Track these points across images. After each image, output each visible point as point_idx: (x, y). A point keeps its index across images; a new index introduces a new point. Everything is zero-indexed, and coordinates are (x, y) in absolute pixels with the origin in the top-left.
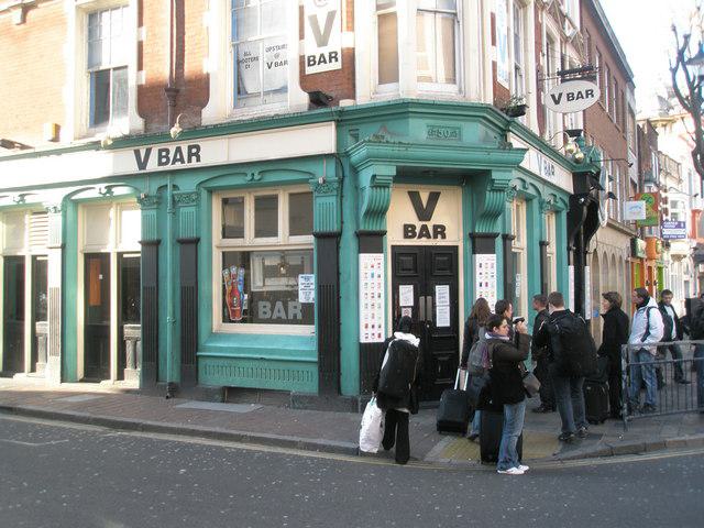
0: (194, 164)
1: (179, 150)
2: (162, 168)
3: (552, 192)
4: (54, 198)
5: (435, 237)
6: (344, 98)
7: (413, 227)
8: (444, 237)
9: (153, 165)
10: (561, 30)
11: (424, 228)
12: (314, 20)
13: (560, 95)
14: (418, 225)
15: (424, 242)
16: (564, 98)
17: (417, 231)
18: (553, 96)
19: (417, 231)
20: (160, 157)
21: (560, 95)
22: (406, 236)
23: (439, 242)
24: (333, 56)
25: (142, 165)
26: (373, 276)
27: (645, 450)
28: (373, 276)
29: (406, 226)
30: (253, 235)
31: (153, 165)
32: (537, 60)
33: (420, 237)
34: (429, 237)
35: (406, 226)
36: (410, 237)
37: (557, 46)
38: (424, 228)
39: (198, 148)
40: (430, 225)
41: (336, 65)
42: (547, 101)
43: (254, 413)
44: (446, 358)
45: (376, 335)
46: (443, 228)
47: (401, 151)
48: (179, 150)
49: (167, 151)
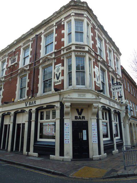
0: (35, 105)
1: (32, 102)
2: (29, 106)
3: (114, 109)
4: (13, 112)
5: (82, 119)
6: (62, 89)
7: (77, 117)
8: (84, 119)
9: (28, 105)
10: (116, 77)
11: (80, 117)
12: (57, 74)
13: (114, 89)
14: (78, 116)
15: (80, 120)
16: (115, 89)
17: (78, 117)
18: (113, 89)
19: (78, 117)
20: (29, 104)
21: (114, 89)
22: (75, 119)
23: (83, 120)
24: (60, 81)
25: (26, 105)
26: (67, 128)
27: (129, 176)
28: (67, 128)
29: (75, 117)
30: (51, 118)
31: (28, 105)
32: (109, 81)
33: (79, 119)
34: (81, 119)
35: (75, 117)
36: (77, 119)
37: (115, 80)
38: (80, 117)
39: (35, 101)
40: (81, 116)
41: (60, 83)
42: (111, 90)
43: (41, 161)
44: (86, 148)
45: (68, 142)
46: (84, 117)
47: (72, 100)
48: (32, 102)
49: (30, 102)
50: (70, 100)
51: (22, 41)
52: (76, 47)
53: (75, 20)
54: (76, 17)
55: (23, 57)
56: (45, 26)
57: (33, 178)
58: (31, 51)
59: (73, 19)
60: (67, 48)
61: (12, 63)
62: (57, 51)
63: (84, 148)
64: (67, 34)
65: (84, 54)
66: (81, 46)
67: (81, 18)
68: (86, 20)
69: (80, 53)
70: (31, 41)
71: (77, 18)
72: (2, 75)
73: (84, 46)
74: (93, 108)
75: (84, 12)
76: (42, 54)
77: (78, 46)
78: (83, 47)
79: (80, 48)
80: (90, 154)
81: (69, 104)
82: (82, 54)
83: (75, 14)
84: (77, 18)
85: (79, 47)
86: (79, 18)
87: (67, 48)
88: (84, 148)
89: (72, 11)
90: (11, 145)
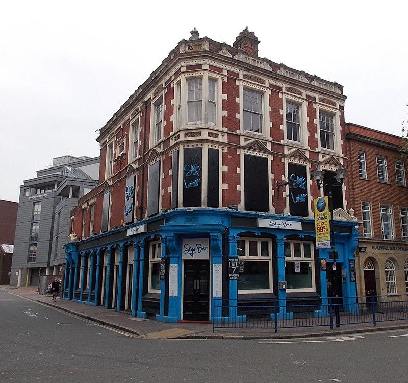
50: (174, 228)
51: (130, 110)
52: (187, 135)
53: (187, 79)
54: (188, 74)
55: (155, 123)
56: (153, 86)
57: (194, 344)
58: (165, 112)
59: (182, 78)
60: (187, 132)
61: (120, 151)
63: (202, 304)
65: (199, 146)
67: (197, 75)
68: (206, 76)
69: (197, 145)
70: (165, 88)
71: (191, 75)
72: (136, 156)
73: (198, 131)
75: (202, 61)
76: (152, 143)
77: (190, 131)
79: (194, 134)
80: (322, 281)
81: (171, 235)
82: (195, 146)
83: (187, 67)
84: (191, 75)
86: (194, 74)
87: (187, 132)
88: (202, 304)
89: (182, 63)
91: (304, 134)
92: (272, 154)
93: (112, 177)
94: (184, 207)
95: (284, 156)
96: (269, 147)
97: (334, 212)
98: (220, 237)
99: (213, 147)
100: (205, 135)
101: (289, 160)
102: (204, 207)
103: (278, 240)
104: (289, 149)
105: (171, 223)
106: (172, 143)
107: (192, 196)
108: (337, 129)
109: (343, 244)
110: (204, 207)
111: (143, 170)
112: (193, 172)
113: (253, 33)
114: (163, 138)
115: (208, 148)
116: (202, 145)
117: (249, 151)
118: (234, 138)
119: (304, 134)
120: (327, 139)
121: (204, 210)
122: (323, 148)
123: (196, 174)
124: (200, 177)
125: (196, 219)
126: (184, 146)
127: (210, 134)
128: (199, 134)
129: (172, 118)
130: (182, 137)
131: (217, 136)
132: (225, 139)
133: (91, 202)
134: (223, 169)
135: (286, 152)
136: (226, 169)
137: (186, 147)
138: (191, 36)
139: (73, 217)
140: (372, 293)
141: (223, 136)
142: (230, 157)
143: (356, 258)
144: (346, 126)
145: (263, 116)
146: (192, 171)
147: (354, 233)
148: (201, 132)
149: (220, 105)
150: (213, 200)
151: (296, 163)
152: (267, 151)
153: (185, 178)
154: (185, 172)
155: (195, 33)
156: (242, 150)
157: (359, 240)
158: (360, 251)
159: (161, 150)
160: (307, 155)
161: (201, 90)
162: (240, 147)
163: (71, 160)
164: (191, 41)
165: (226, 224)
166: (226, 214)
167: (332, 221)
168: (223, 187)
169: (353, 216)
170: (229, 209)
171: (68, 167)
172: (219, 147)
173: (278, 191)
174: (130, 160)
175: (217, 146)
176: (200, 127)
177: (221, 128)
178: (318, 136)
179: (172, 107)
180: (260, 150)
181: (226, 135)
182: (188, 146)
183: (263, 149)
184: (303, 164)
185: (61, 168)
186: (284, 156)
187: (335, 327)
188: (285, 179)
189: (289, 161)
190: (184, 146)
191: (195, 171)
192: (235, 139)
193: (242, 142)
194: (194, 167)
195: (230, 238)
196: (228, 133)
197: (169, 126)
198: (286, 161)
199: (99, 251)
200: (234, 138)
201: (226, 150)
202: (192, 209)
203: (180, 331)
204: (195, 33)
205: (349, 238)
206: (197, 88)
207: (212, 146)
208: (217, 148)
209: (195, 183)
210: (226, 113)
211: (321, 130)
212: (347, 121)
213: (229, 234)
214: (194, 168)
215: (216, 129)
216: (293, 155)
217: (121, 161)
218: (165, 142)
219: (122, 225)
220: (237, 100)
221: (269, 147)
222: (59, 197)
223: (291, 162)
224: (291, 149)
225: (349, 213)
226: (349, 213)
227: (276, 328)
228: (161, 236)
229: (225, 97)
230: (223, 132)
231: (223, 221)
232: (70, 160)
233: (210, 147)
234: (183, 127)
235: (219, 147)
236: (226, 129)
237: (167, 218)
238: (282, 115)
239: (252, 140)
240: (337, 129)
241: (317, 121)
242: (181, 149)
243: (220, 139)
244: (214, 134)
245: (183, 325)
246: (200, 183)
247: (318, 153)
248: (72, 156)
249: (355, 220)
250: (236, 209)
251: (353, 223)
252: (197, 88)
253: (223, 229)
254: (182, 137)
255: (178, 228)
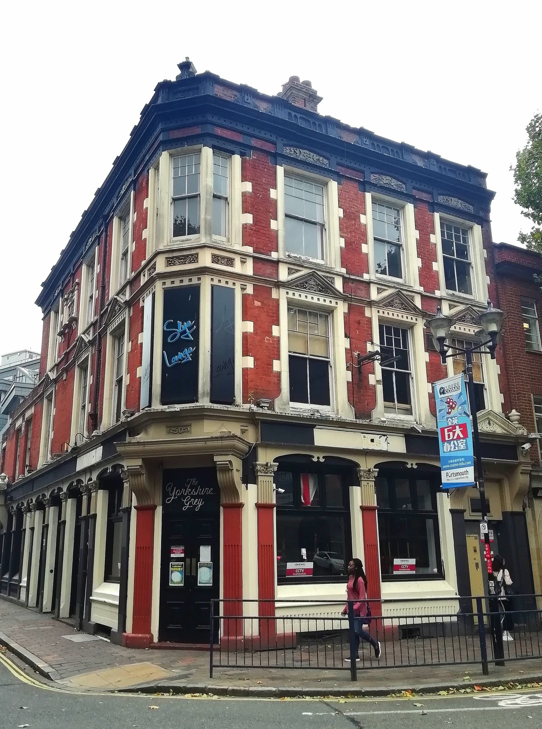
50: (140, 448)
52: (170, 262)
60: (171, 255)
62: (136, 273)
64: (171, 200)
65: (195, 281)
66: (185, 253)
73: (193, 252)
74: (520, 471)
77: (175, 254)
78: (192, 255)
79: (184, 259)
81: (139, 462)
82: (186, 282)
85: (178, 257)
87: (171, 255)
90: (126, 596)
91: (412, 264)
92: (345, 299)
93: (56, 365)
94: (163, 405)
95: (371, 304)
96: (339, 285)
97: (478, 414)
98: (237, 464)
99: (223, 284)
100: (205, 259)
101: (381, 311)
102: (204, 402)
103: (362, 473)
104: (379, 291)
105: (141, 437)
106: (143, 280)
107: (179, 381)
108: (477, 255)
109: (499, 482)
110: (204, 402)
111: (100, 345)
112: (182, 333)
113: (307, 84)
114: (130, 275)
115: (213, 287)
116: (199, 279)
117: (297, 294)
118: (265, 264)
119: (412, 264)
120: (458, 273)
121: (203, 409)
122: (451, 292)
123: (188, 336)
124: (196, 343)
125: (186, 429)
126: (164, 283)
127: (216, 259)
128: (195, 258)
129: (145, 234)
130: (161, 266)
131: (230, 262)
132: (249, 269)
133: (28, 414)
134: (243, 327)
135: (374, 295)
136: (249, 327)
137: (168, 285)
138: (180, 72)
139: (5, 445)
140: (397, 636)
141: (243, 262)
142: (257, 303)
143: (528, 511)
144: (496, 251)
145: (327, 226)
146: (179, 330)
147: (521, 459)
148: (197, 254)
149: (237, 202)
150: (222, 391)
151: (395, 317)
152: (335, 294)
153: (165, 346)
154: (165, 334)
155: (185, 66)
156: (283, 291)
157: (533, 473)
158: (537, 497)
159: (127, 297)
160: (418, 302)
161: (198, 174)
162: (279, 285)
163: (31, 357)
164: (180, 81)
165: (251, 436)
166: (251, 418)
167: (476, 434)
168: (243, 362)
169: (517, 426)
170: (255, 408)
171: (23, 369)
172: (234, 284)
173: (360, 373)
174: (81, 327)
175: (231, 282)
176: (195, 244)
177: (238, 246)
178: (438, 266)
179: (144, 211)
180: (320, 291)
181: (250, 262)
182: (173, 282)
183: (326, 288)
184: (409, 320)
185: (12, 370)
186: (371, 304)
187: (491, 667)
188: (374, 347)
189: (381, 314)
190: (164, 283)
191: (185, 332)
192: (268, 270)
193: (283, 275)
194: (183, 324)
195: (258, 468)
196: (254, 258)
197: (141, 244)
198: (373, 315)
199: (34, 502)
200: (265, 264)
201: (250, 290)
202: (177, 407)
203: (148, 669)
204: (185, 66)
205: (511, 470)
206: (190, 171)
207: (220, 281)
208: (230, 285)
209: (185, 354)
210: (249, 219)
211: (444, 257)
212: (497, 239)
213: (256, 459)
214: (183, 326)
215: (229, 247)
216: (388, 303)
217: (68, 331)
218: (132, 282)
219: (67, 451)
220: (273, 194)
221: (339, 285)
222: (5, 416)
223: (386, 315)
224: (385, 290)
225: (508, 418)
226: (508, 418)
227: (353, 669)
228: (122, 466)
229: (248, 187)
230: (244, 256)
231: (243, 431)
232: (28, 357)
233: (216, 282)
234: (161, 248)
235: (234, 284)
236: (249, 250)
237: (132, 428)
238: (365, 225)
239: (304, 272)
240: (477, 255)
241: (436, 239)
242: (159, 288)
243: (237, 268)
244: (223, 258)
245: (158, 653)
246: (196, 355)
247: (440, 300)
248: (32, 350)
249: (522, 431)
250: (271, 407)
251: (518, 438)
252: (190, 171)
253: (246, 448)
254: (161, 266)
255: (147, 447)
